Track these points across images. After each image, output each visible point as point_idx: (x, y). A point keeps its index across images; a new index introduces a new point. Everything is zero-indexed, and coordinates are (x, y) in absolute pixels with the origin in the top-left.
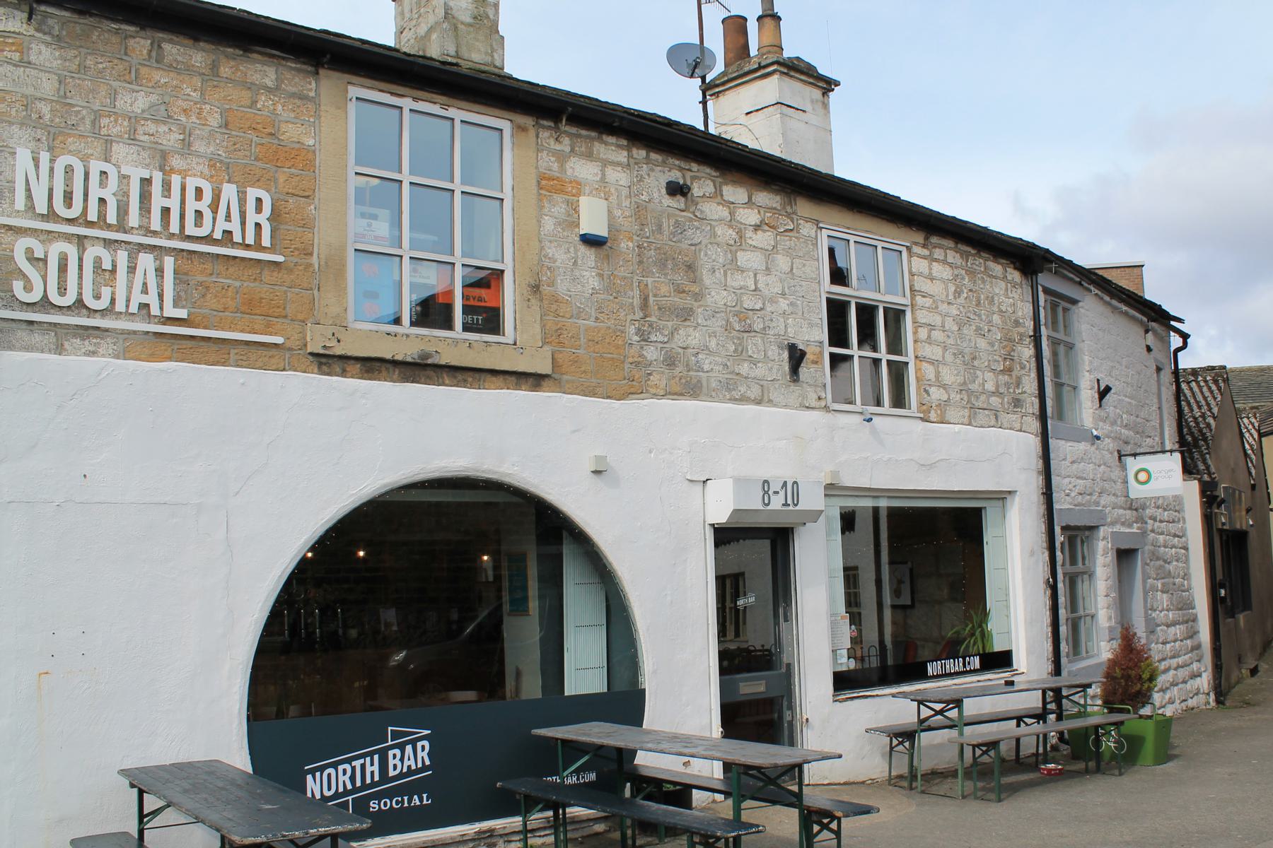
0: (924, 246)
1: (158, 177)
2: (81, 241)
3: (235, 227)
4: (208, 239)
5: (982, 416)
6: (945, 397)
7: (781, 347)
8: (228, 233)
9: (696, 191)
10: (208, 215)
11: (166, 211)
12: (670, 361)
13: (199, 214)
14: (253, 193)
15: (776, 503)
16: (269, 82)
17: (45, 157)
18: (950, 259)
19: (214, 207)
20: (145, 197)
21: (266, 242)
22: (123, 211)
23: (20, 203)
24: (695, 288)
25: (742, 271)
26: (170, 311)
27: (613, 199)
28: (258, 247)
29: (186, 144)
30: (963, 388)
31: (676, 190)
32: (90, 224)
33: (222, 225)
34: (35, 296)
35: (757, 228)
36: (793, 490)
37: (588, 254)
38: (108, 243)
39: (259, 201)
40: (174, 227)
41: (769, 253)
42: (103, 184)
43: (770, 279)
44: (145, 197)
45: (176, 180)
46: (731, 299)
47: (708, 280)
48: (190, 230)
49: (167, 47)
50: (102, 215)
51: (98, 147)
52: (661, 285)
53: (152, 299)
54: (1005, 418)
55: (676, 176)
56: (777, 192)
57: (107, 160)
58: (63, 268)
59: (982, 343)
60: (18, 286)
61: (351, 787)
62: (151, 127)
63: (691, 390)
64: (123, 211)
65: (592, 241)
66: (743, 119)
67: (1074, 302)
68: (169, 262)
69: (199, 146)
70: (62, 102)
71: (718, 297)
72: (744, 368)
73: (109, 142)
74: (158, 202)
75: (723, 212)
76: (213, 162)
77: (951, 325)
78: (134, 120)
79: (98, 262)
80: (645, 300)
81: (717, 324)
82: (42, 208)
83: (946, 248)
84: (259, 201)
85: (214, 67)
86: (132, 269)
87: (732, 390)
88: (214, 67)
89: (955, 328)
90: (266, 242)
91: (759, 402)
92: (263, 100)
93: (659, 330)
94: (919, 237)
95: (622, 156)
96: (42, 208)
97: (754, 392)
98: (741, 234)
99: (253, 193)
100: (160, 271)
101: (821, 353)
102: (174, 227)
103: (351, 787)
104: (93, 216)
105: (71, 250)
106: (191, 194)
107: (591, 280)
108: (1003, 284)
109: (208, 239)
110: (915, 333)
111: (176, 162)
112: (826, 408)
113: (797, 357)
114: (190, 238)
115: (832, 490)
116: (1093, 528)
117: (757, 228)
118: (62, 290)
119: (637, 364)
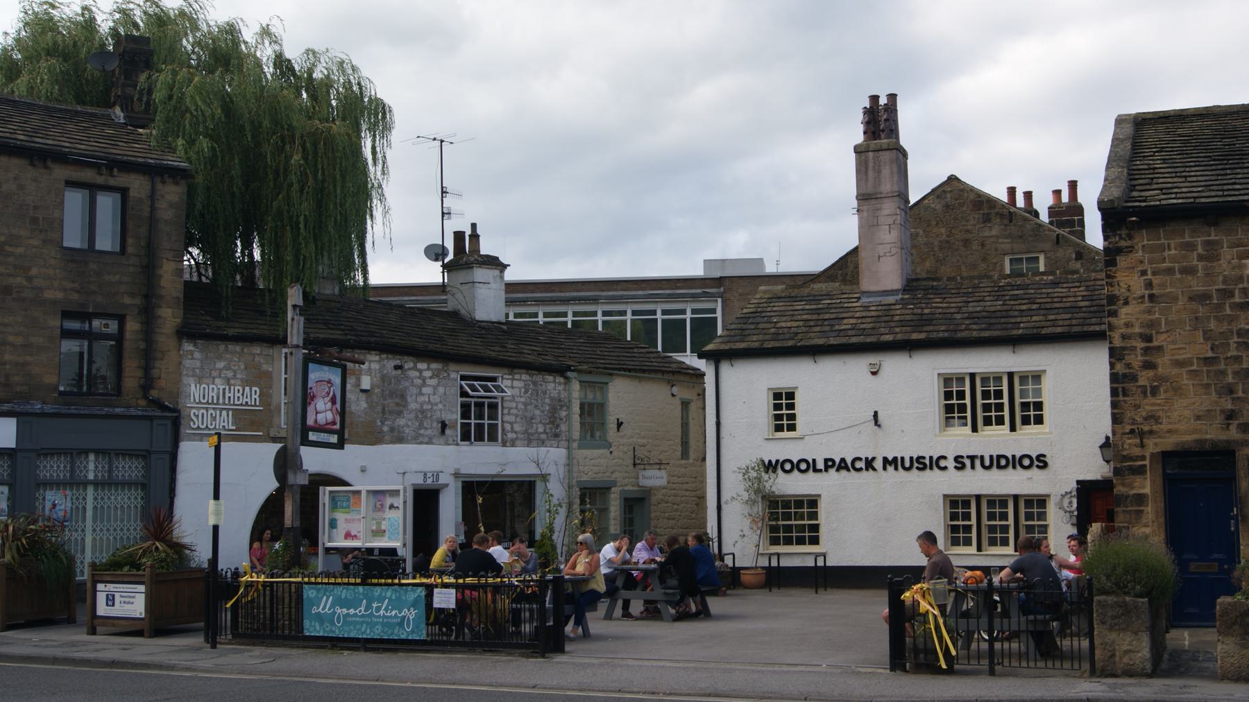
0: (509, 374)
1: (227, 387)
2: (207, 409)
3: (249, 400)
4: (241, 405)
5: (534, 443)
6: (515, 436)
7: (438, 422)
8: (247, 402)
9: (406, 367)
10: (241, 397)
11: (229, 397)
12: (392, 430)
13: (239, 397)
14: (254, 389)
15: (429, 481)
16: (258, 352)
17: (198, 385)
18: (523, 378)
19: (243, 395)
20: (224, 393)
21: (258, 404)
22: (218, 398)
23: (192, 400)
24: (404, 403)
25: (424, 395)
26: (231, 427)
27: (373, 374)
28: (255, 405)
29: (235, 375)
30: (526, 432)
31: (397, 368)
32: (210, 404)
33: (245, 400)
34: (195, 426)
35: (431, 378)
36: (437, 475)
37: (363, 396)
38: (214, 408)
39: (256, 391)
40: (232, 402)
41: (435, 388)
42: (213, 392)
43: (435, 397)
44: (224, 393)
45: (232, 387)
46: (418, 406)
47: (409, 399)
48: (236, 402)
49: (229, 346)
50: (213, 400)
51: (211, 380)
52: (390, 403)
53: (226, 424)
54: (548, 443)
55: (398, 362)
56: (440, 363)
57: (213, 384)
58: (203, 417)
59: (537, 412)
60: (192, 423)
61: (336, 436)
62: (225, 372)
63: (400, 440)
64: (218, 398)
65: (363, 391)
66: (459, 286)
67: (607, 383)
68: (230, 413)
69: (238, 376)
70: (202, 368)
71: (413, 406)
72: (422, 431)
73: (214, 378)
74: (227, 395)
75: (417, 374)
76: (242, 380)
77: (521, 406)
78: (221, 370)
79: (212, 414)
80: (384, 409)
81: (412, 416)
82: (197, 401)
83: (521, 374)
84: (256, 391)
85: (242, 350)
86: (220, 416)
87: (417, 439)
88: (242, 350)
89: (523, 407)
90: (258, 404)
91: (427, 443)
92: (257, 359)
93: (388, 420)
94: (506, 371)
95: (377, 358)
96: (197, 401)
97: (426, 439)
98: (424, 381)
99: (254, 389)
100: (228, 415)
101: (457, 423)
102: (232, 402)
103: (336, 436)
104: (210, 401)
105: (204, 411)
106: (236, 390)
107: (364, 405)
108: (553, 385)
109: (241, 405)
110: (502, 411)
111: (232, 382)
112: (457, 444)
113: (444, 426)
114: (237, 405)
115: (457, 475)
116: (609, 488)
117: (431, 378)
118: (203, 424)
119: (380, 432)
